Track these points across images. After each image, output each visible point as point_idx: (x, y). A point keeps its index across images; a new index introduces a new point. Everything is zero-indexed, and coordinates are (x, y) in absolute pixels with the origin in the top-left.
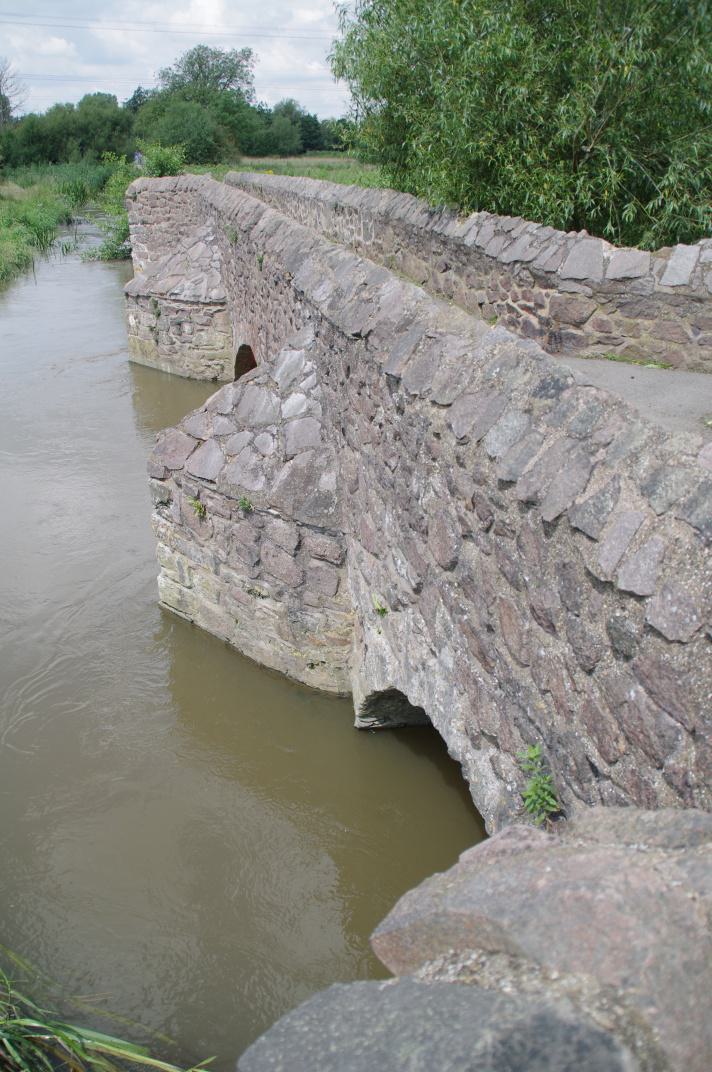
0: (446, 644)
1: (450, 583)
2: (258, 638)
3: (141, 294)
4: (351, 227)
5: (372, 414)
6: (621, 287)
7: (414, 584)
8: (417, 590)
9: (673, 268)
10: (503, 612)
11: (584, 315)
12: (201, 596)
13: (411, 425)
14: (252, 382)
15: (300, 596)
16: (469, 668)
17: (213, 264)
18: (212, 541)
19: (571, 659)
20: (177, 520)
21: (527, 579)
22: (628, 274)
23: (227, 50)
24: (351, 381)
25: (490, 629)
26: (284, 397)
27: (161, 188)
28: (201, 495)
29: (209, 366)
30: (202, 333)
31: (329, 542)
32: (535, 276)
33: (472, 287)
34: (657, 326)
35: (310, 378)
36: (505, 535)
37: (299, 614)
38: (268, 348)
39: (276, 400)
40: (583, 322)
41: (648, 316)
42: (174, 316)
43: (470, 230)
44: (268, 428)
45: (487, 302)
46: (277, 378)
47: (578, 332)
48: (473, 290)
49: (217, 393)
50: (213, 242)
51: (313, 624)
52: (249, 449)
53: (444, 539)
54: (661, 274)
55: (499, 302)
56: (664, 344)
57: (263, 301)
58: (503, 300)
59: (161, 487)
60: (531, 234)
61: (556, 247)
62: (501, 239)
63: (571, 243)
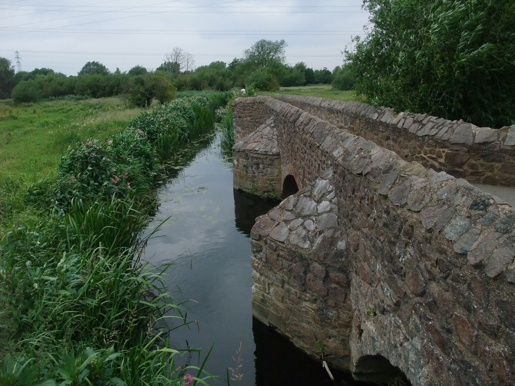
0: (416, 335)
1: (421, 304)
2: (302, 321)
3: (240, 150)
4: (337, 119)
5: (369, 213)
6: (483, 147)
7: (394, 301)
8: (397, 304)
9: (511, 137)
10: (458, 323)
11: (463, 161)
12: (274, 298)
13: (395, 220)
14: (302, 195)
15: (326, 301)
16: (433, 351)
17: (274, 137)
18: (281, 272)
19: (510, 355)
20: (264, 260)
21: (476, 307)
22: (486, 140)
23: (274, 41)
24: (355, 197)
25: (449, 331)
26: (319, 202)
27: (248, 102)
28: (278, 249)
29: (271, 184)
30: (268, 169)
31: (342, 275)
32: (437, 142)
33: (402, 148)
34: (503, 166)
35: (332, 193)
36: (459, 282)
37: (324, 310)
38: (304, 177)
39: (315, 204)
40: (463, 164)
41: (497, 162)
42: (255, 160)
43: (400, 120)
44: (311, 218)
45: (410, 155)
46: (315, 193)
47: (461, 170)
48: (402, 149)
49: (285, 200)
50: (273, 127)
51: (331, 316)
52: (301, 227)
53: (417, 280)
54: (504, 140)
55: (417, 155)
56: (507, 175)
57: (302, 155)
58: (419, 154)
59: (257, 244)
60: (433, 122)
61: (447, 128)
62: (417, 125)
63: (455, 126)
